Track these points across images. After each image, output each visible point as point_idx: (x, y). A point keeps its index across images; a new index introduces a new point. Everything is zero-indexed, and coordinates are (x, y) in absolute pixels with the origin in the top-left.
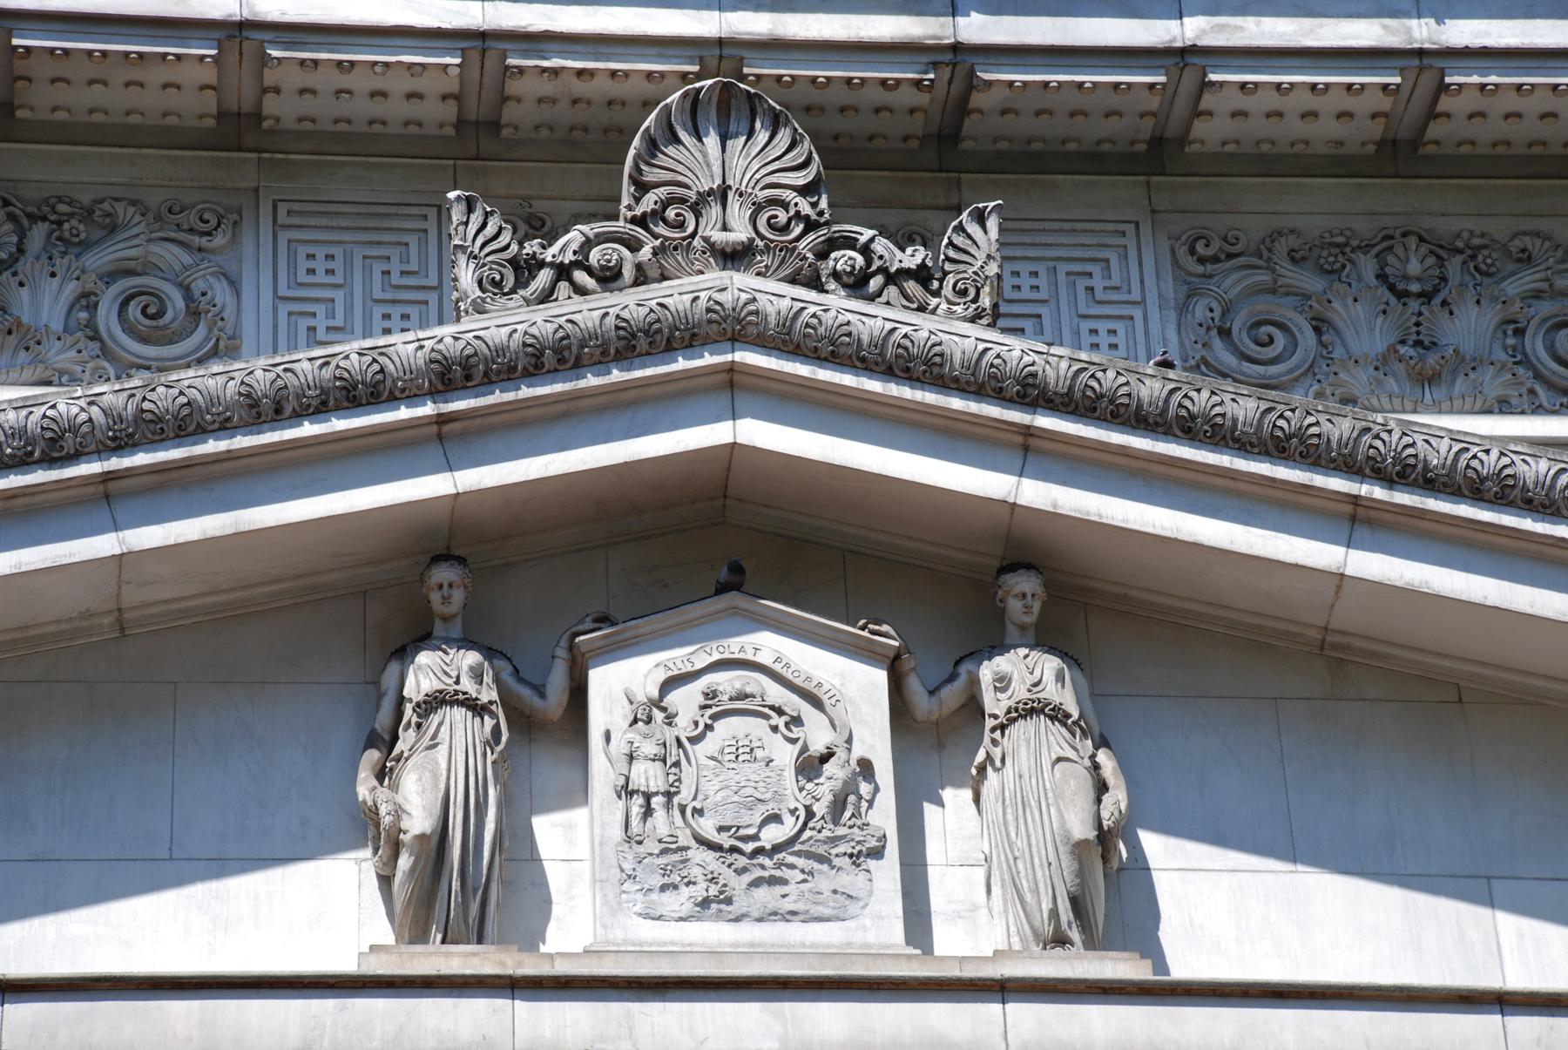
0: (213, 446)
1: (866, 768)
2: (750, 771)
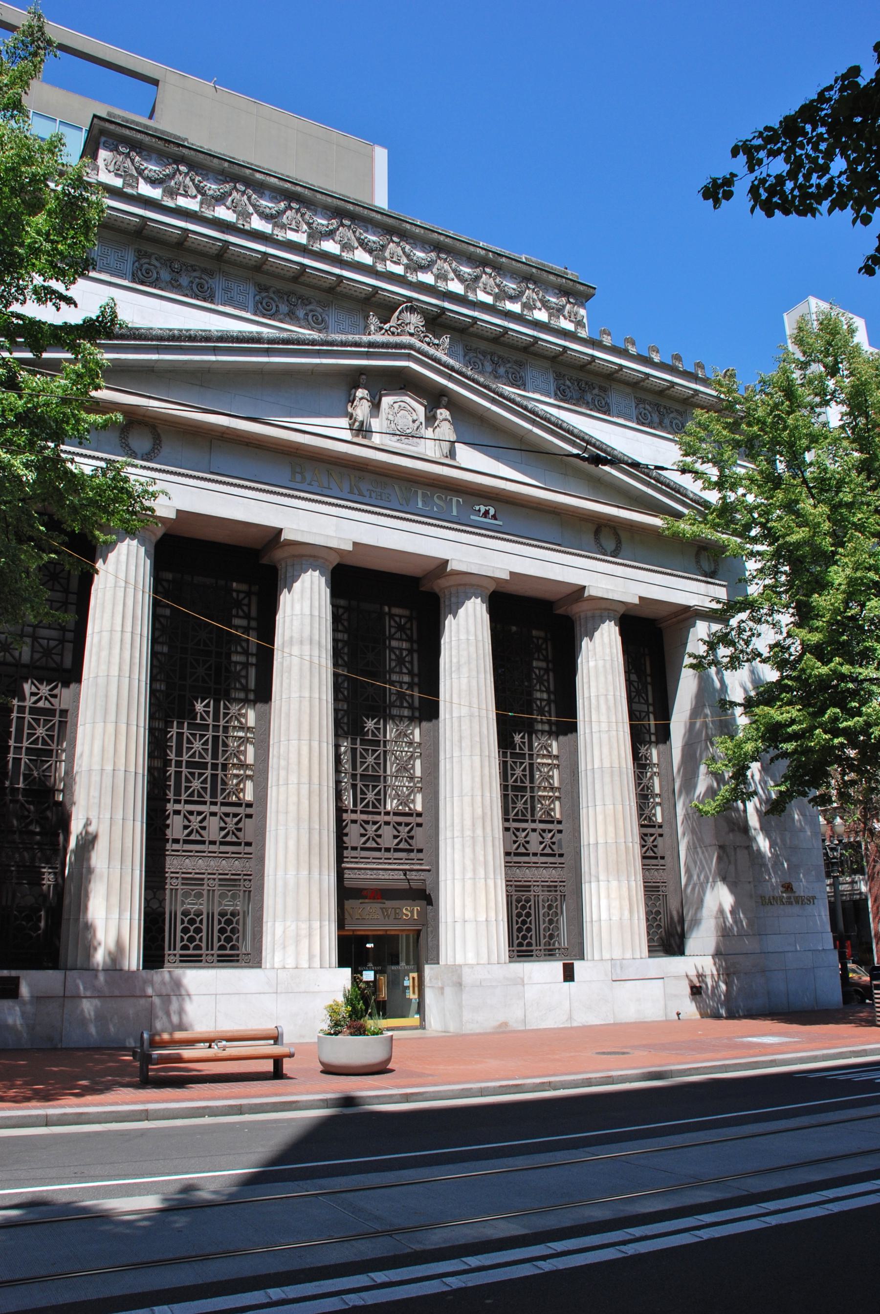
0: (335, 348)
1: (421, 423)
2: (404, 421)
